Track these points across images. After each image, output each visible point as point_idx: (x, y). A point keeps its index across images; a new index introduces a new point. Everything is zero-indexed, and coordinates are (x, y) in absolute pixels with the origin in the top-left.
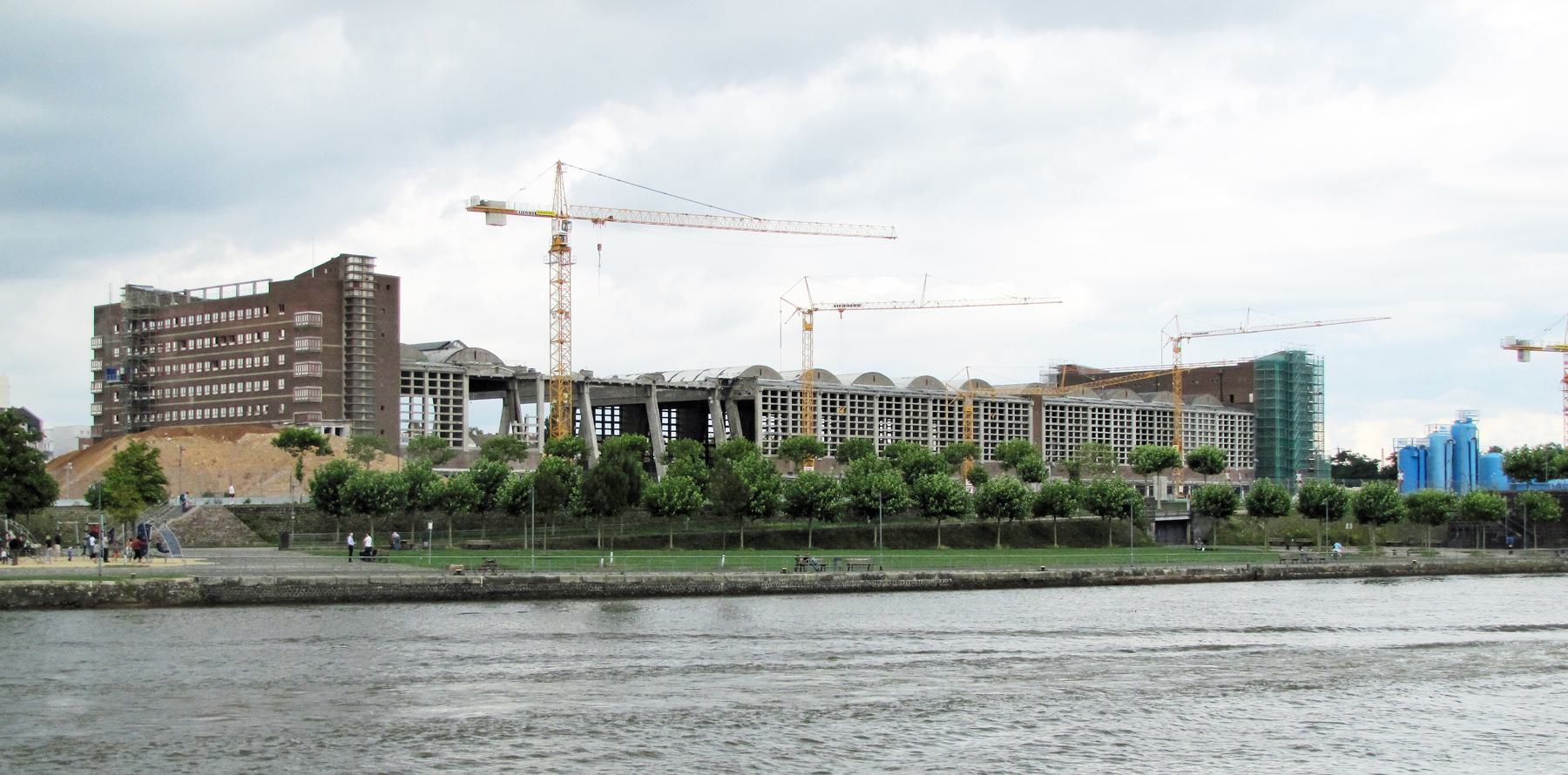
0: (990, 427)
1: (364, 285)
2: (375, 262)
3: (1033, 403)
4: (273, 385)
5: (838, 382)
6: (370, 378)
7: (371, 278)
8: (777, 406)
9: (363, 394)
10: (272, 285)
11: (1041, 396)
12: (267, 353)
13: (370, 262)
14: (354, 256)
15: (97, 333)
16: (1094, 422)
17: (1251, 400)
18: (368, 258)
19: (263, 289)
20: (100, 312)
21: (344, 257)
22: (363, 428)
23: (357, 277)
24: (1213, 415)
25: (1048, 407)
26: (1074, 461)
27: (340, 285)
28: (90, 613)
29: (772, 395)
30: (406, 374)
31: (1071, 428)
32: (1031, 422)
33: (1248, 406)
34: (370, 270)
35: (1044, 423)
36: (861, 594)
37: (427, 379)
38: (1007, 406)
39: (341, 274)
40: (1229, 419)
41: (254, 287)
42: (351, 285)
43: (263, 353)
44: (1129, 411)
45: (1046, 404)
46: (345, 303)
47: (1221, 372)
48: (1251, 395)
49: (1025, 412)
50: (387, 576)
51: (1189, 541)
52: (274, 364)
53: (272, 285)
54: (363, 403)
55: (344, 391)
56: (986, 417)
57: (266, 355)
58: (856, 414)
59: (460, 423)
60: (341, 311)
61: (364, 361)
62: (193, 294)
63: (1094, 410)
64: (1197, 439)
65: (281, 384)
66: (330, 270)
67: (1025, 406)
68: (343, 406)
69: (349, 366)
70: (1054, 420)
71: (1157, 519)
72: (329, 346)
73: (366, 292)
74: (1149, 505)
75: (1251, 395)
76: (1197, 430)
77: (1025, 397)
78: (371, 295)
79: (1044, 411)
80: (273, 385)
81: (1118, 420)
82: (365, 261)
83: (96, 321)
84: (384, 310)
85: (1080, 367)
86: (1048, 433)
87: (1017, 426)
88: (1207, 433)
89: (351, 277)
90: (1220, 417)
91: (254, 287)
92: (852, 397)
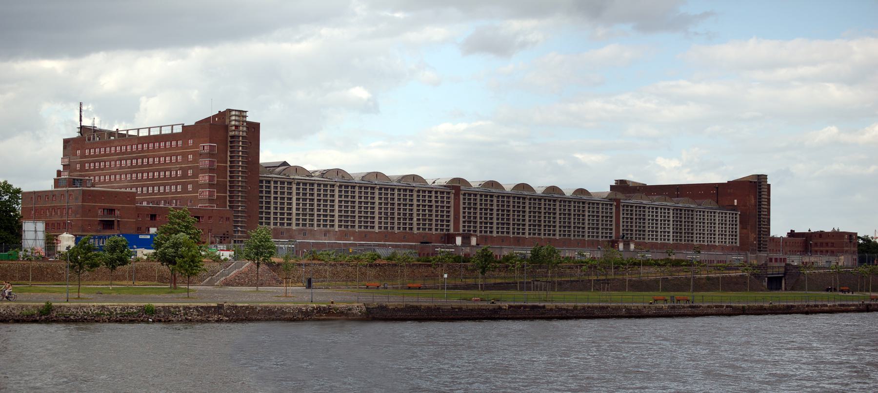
0: (402, 207)
1: (241, 128)
2: (248, 114)
3: (454, 191)
4: (185, 190)
5: (504, 189)
6: (244, 184)
7: (245, 124)
8: (471, 203)
9: (240, 194)
10: (184, 127)
11: (620, 200)
12: (181, 169)
13: (244, 114)
14: (236, 110)
15: (65, 155)
16: (649, 215)
17: (736, 204)
18: (243, 111)
19: (178, 130)
20: (66, 142)
21: (230, 111)
22: (240, 214)
23: (237, 123)
24: (715, 213)
25: (464, 195)
26: (466, 232)
27: (226, 128)
28: (61, 326)
29: (490, 197)
30: (262, 182)
31: (636, 219)
32: (614, 215)
33: (734, 208)
34: (244, 119)
35: (621, 216)
36: (450, 322)
37: (272, 185)
38: (433, 193)
39: (227, 121)
40: (734, 216)
41: (172, 129)
42: (233, 128)
43: (178, 169)
44: (669, 209)
45: (623, 204)
46: (229, 139)
47: (717, 186)
48: (736, 201)
49: (448, 198)
50: (726, 295)
51: (783, 289)
52: (185, 175)
53: (184, 127)
54: (240, 199)
55: (228, 192)
56: (418, 201)
57: (179, 170)
58: (439, 204)
59: (291, 212)
60: (756, 197)
61: (240, 174)
62: (130, 133)
63: (649, 208)
64: (600, 220)
65: (190, 187)
66: (219, 119)
67: (448, 193)
68: (228, 202)
69: (759, 218)
70: (627, 214)
71: (769, 276)
72: (220, 164)
73: (242, 132)
74: (764, 268)
75: (736, 201)
76: (706, 221)
77: (611, 200)
78: (245, 134)
79: (461, 197)
80: (185, 190)
81: (651, 214)
82: (242, 114)
83: (65, 148)
84: (251, 143)
85: (629, 181)
86: (464, 213)
87: (442, 207)
88: (711, 223)
89: (233, 123)
90: (719, 213)
91: (172, 129)
92: (481, 195)
